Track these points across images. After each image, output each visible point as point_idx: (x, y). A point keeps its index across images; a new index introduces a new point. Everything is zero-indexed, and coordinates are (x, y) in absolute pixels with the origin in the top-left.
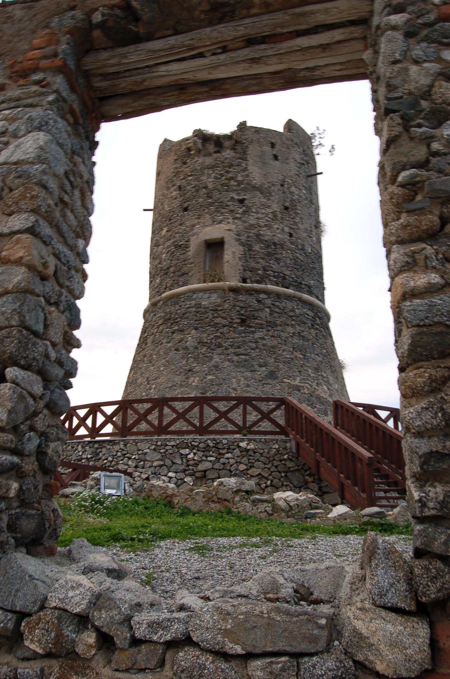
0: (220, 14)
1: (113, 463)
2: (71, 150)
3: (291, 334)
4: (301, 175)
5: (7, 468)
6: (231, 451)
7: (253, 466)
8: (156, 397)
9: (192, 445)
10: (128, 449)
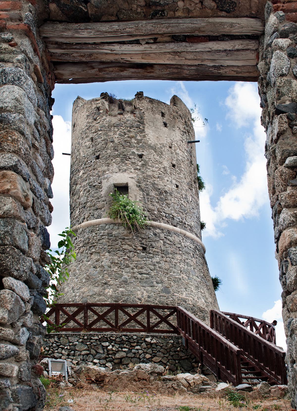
0: (154, 12)
1: (50, 352)
2: (38, 104)
3: (179, 261)
4: (184, 141)
5: (10, 354)
6: (140, 344)
7: (156, 356)
8: (80, 302)
9: (110, 339)
10: (61, 342)
